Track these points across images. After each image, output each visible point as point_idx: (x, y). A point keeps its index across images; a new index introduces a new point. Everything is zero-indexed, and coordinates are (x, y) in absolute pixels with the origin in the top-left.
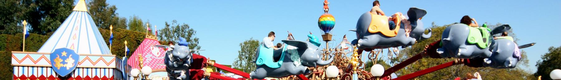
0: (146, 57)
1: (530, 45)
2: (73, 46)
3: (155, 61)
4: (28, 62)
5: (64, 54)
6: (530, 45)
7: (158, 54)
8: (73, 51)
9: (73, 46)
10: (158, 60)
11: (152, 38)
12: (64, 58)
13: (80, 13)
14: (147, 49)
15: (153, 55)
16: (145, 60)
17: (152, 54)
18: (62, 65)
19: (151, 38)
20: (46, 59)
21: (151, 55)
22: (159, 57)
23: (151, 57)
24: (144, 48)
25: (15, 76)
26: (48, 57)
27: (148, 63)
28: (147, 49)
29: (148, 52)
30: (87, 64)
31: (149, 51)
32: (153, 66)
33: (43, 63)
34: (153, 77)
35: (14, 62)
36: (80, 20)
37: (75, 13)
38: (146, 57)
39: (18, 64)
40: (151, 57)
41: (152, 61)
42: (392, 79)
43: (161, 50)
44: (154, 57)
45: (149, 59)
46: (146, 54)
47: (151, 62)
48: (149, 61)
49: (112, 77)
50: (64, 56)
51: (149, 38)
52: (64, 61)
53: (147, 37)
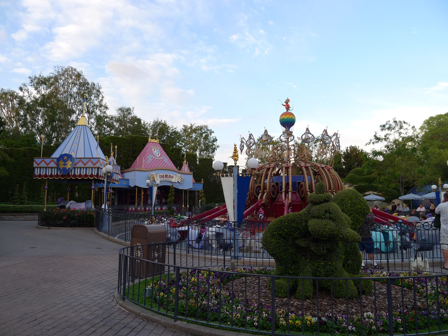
0: (148, 157)
1: (96, 248)
2: (73, 152)
3: (156, 161)
4: (43, 164)
5: (65, 158)
6: (96, 248)
7: (158, 154)
8: (71, 156)
9: (73, 152)
10: (158, 160)
11: (155, 141)
12: (65, 161)
13: (81, 126)
14: (149, 151)
15: (154, 156)
16: (147, 160)
17: (154, 155)
18: (64, 166)
19: (153, 141)
20: (54, 162)
21: (152, 156)
22: (159, 157)
23: (152, 158)
24: (146, 150)
25: (35, 174)
26: (55, 160)
27: (149, 163)
28: (149, 151)
29: (150, 153)
30: (80, 165)
31: (151, 153)
32: (149, 166)
33: (53, 165)
34: (151, 175)
35: (35, 165)
36: (80, 132)
37: (79, 127)
38: (148, 157)
39: (37, 166)
40: (152, 158)
41: (153, 161)
42: (393, 254)
43: (161, 151)
44: (155, 157)
45: (150, 160)
46: (148, 155)
47: (151, 162)
48: (150, 161)
49: (96, 174)
50: (65, 159)
51: (152, 141)
52: (65, 163)
53: (149, 141)
